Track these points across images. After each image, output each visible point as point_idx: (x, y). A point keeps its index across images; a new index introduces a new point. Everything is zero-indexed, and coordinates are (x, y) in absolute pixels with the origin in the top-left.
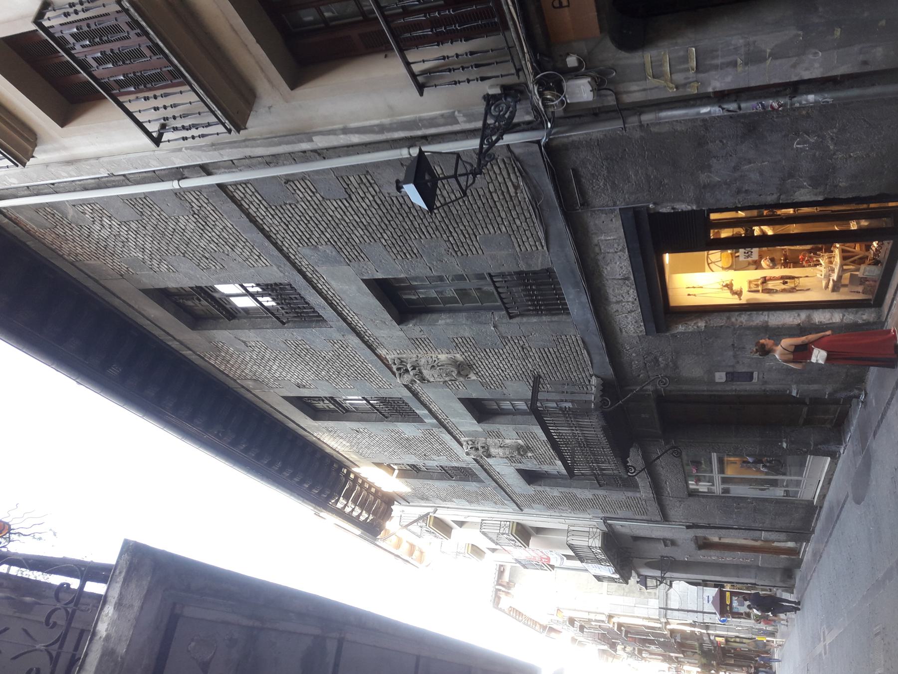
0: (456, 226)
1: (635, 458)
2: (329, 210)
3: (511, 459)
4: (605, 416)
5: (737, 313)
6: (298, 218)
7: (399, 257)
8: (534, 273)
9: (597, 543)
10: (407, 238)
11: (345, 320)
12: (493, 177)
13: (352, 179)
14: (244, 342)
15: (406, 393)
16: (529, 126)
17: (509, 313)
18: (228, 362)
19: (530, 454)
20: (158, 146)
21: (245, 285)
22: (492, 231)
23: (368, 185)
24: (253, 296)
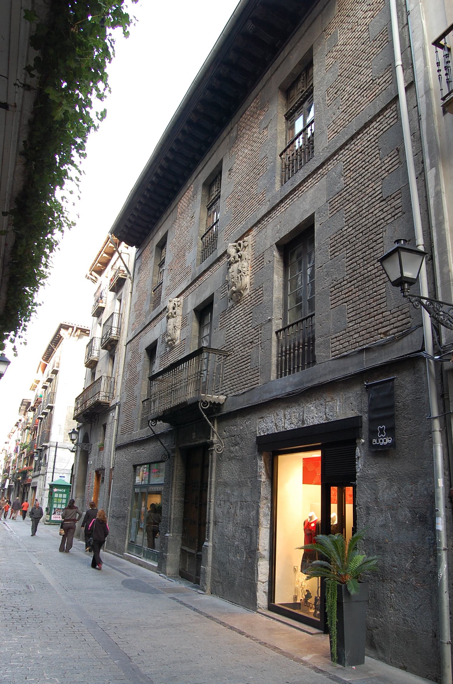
0: (356, 286)
1: (162, 427)
2: (373, 184)
3: (166, 334)
4: (195, 404)
5: (269, 505)
6: (367, 160)
7: (331, 241)
8: (313, 350)
9: (102, 398)
10: (348, 247)
11: (282, 201)
12: (395, 315)
13: (399, 201)
14: (267, 127)
15: (220, 252)
16: (437, 341)
17: (280, 331)
18: (252, 116)
19: (168, 349)
20: (433, 44)
21: (313, 125)
22: (350, 315)
23: (393, 214)
24: (304, 130)
